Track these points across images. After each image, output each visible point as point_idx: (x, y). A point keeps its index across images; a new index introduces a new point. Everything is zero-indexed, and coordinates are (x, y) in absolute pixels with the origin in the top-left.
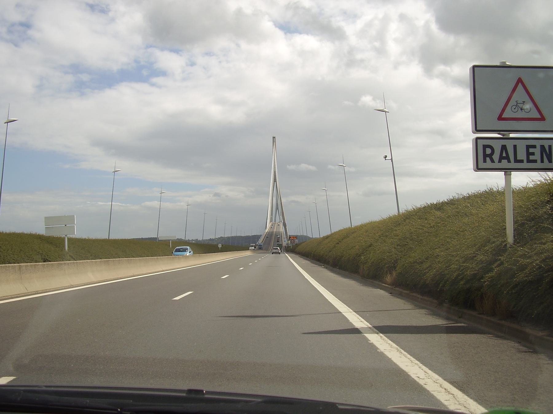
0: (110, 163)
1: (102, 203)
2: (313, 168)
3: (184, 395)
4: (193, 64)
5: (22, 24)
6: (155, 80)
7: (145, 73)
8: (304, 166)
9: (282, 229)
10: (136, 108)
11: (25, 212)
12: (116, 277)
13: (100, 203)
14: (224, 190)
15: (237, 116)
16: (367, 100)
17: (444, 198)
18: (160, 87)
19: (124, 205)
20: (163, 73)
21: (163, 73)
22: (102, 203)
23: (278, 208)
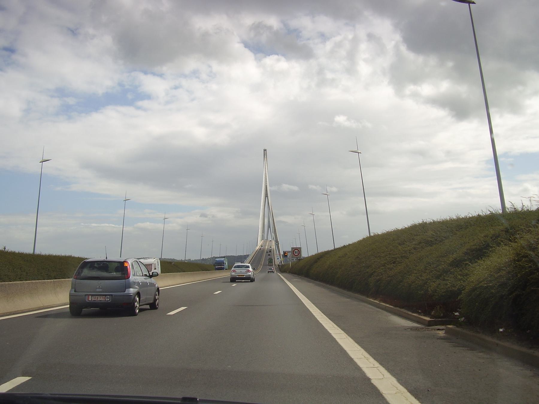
0: (114, 188)
1: (96, 225)
2: (295, 188)
3: (179, 402)
4: (176, 88)
5: (6, 49)
6: (140, 103)
7: (130, 96)
8: (285, 187)
9: (274, 247)
10: (123, 132)
11: (18, 238)
12: (168, 285)
13: (94, 225)
14: (214, 211)
15: (222, 139)
16: (341, 119)
17: (473, 213)
18: (145, 110)
19: (117, 226)
20: (148, 97)
21: (148, 97)
22: (96, 225)
23: (271, 227)
